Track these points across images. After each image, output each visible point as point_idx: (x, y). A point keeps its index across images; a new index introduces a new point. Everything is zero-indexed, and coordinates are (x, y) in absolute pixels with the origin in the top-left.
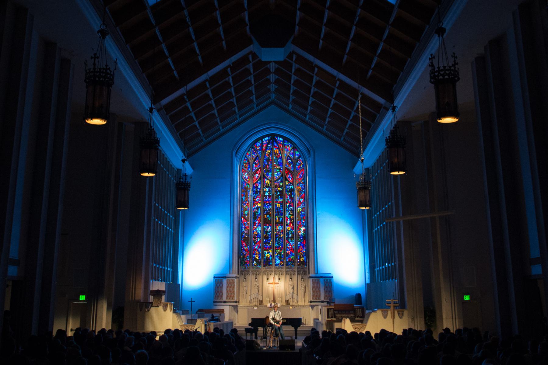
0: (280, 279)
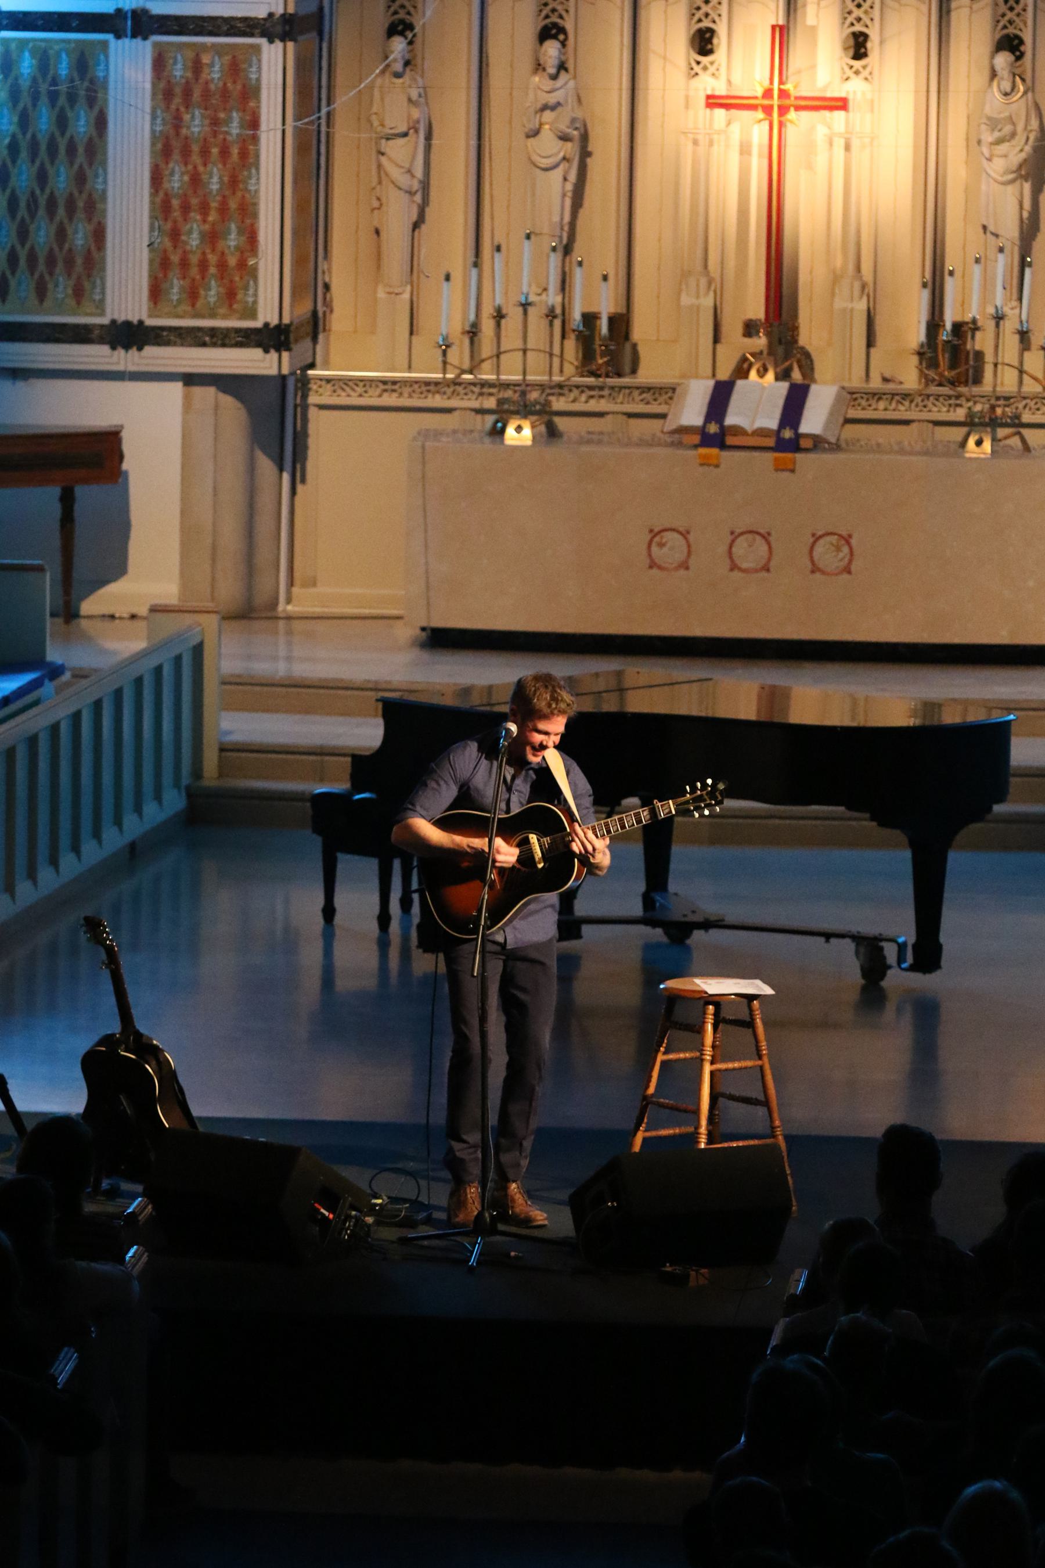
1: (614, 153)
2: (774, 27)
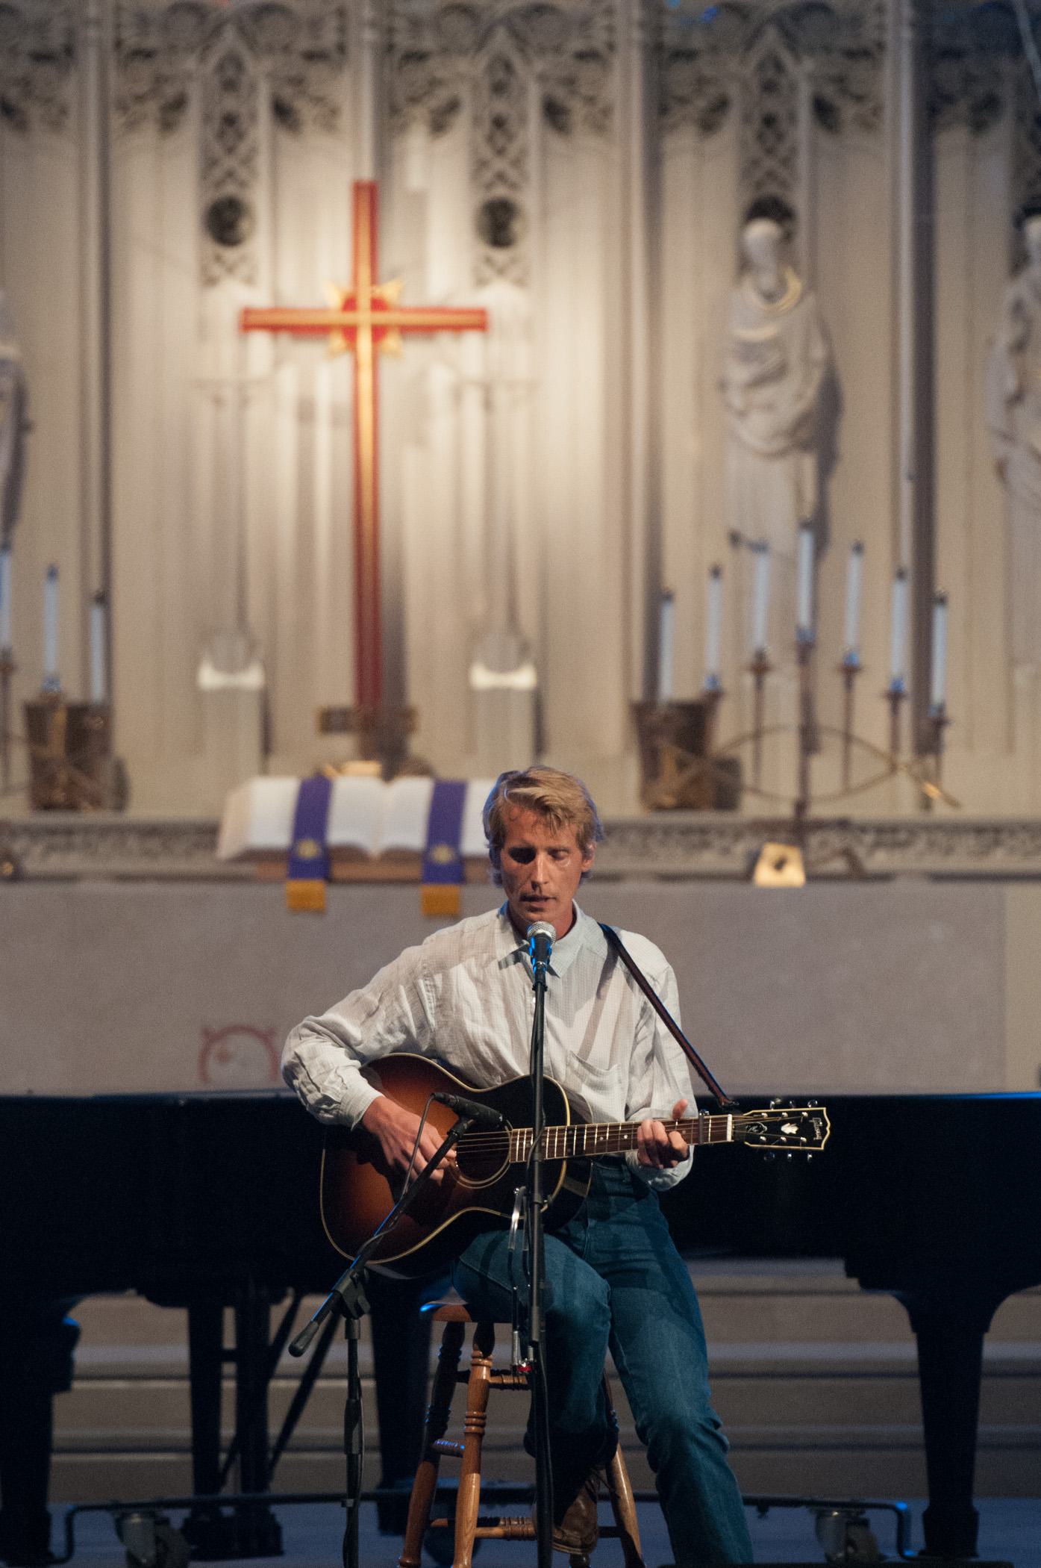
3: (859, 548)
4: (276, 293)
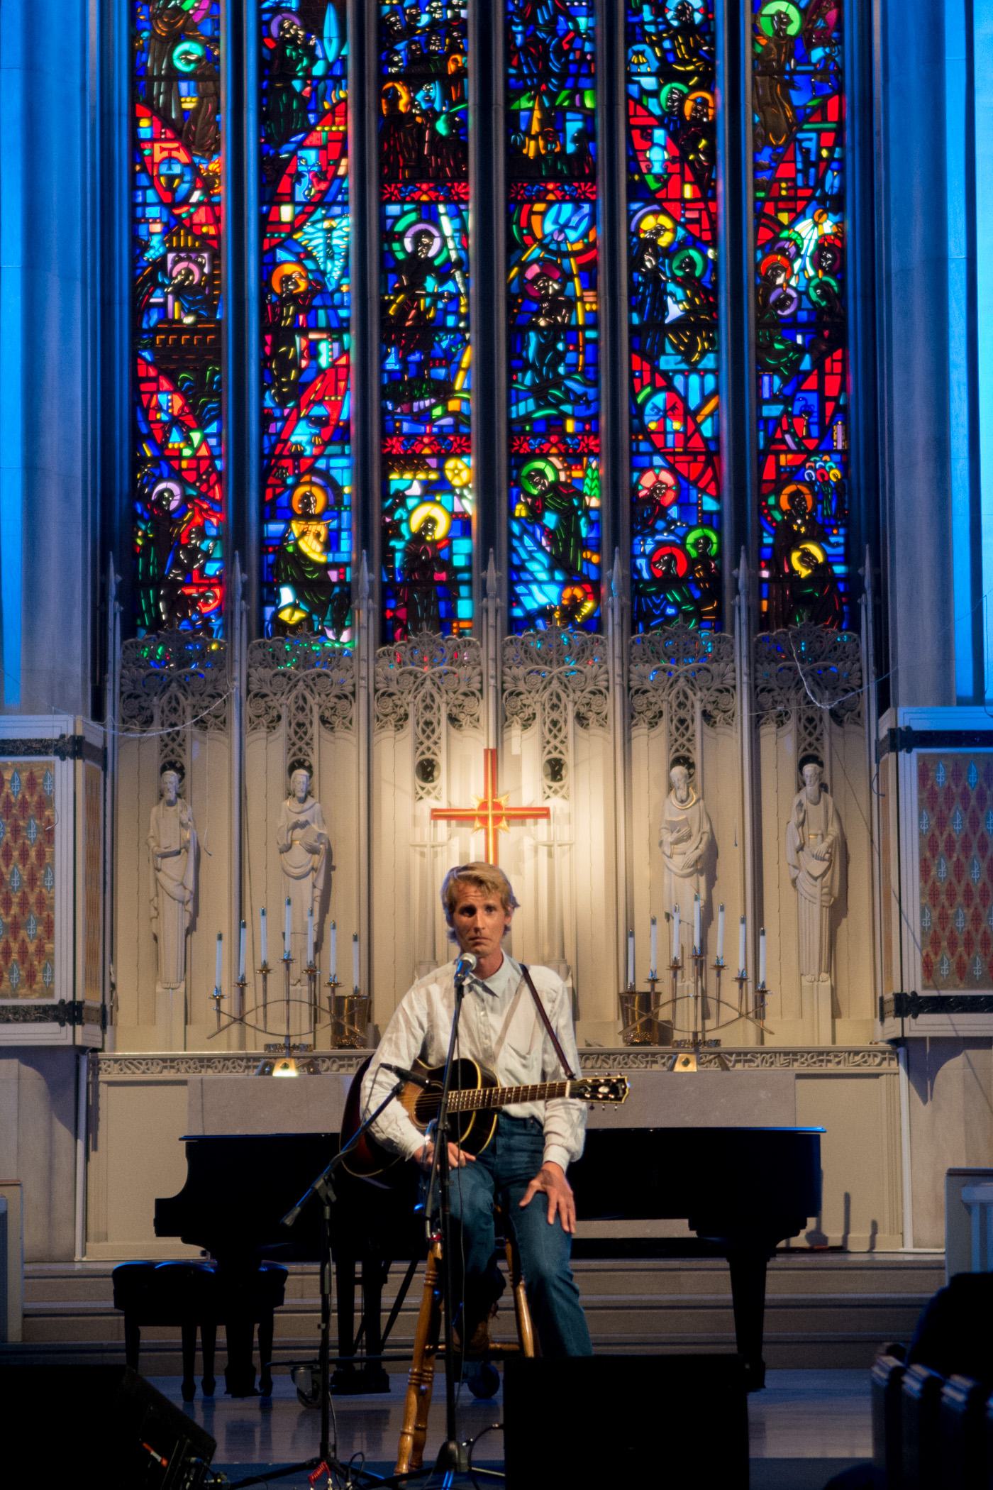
0: (568, 773)
1: (354, 868)
2: (486, 751)
3: (722, 909)
4: (449, 803)
